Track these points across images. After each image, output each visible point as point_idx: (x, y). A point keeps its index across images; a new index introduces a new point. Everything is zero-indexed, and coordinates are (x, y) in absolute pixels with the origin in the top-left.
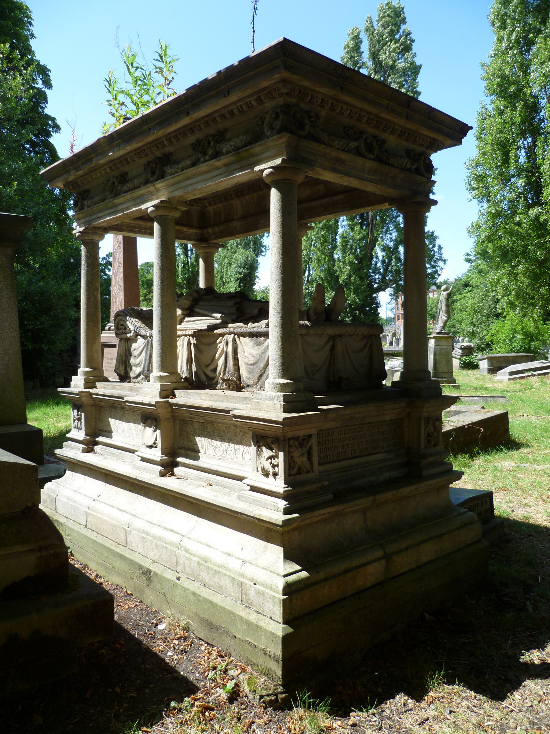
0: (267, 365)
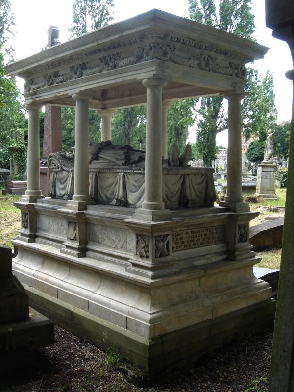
0: (143, 192)
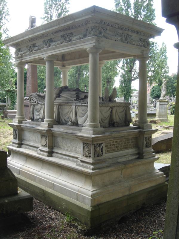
0: (87, 117)
